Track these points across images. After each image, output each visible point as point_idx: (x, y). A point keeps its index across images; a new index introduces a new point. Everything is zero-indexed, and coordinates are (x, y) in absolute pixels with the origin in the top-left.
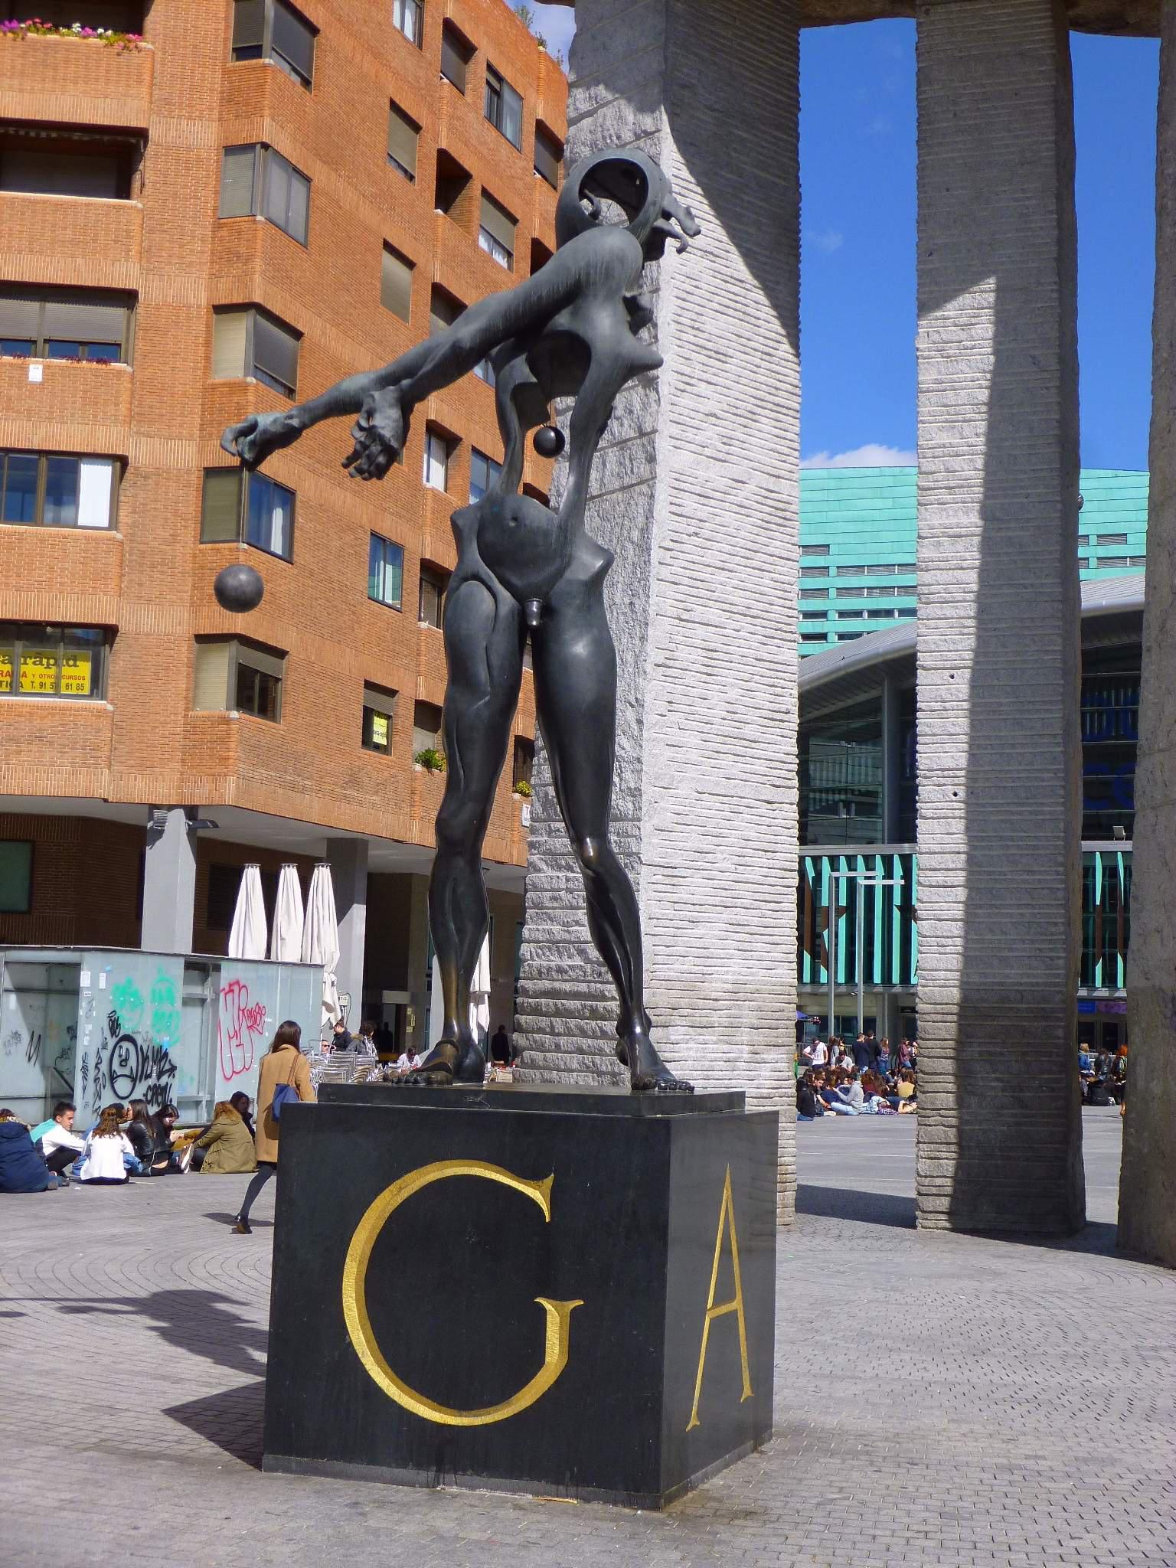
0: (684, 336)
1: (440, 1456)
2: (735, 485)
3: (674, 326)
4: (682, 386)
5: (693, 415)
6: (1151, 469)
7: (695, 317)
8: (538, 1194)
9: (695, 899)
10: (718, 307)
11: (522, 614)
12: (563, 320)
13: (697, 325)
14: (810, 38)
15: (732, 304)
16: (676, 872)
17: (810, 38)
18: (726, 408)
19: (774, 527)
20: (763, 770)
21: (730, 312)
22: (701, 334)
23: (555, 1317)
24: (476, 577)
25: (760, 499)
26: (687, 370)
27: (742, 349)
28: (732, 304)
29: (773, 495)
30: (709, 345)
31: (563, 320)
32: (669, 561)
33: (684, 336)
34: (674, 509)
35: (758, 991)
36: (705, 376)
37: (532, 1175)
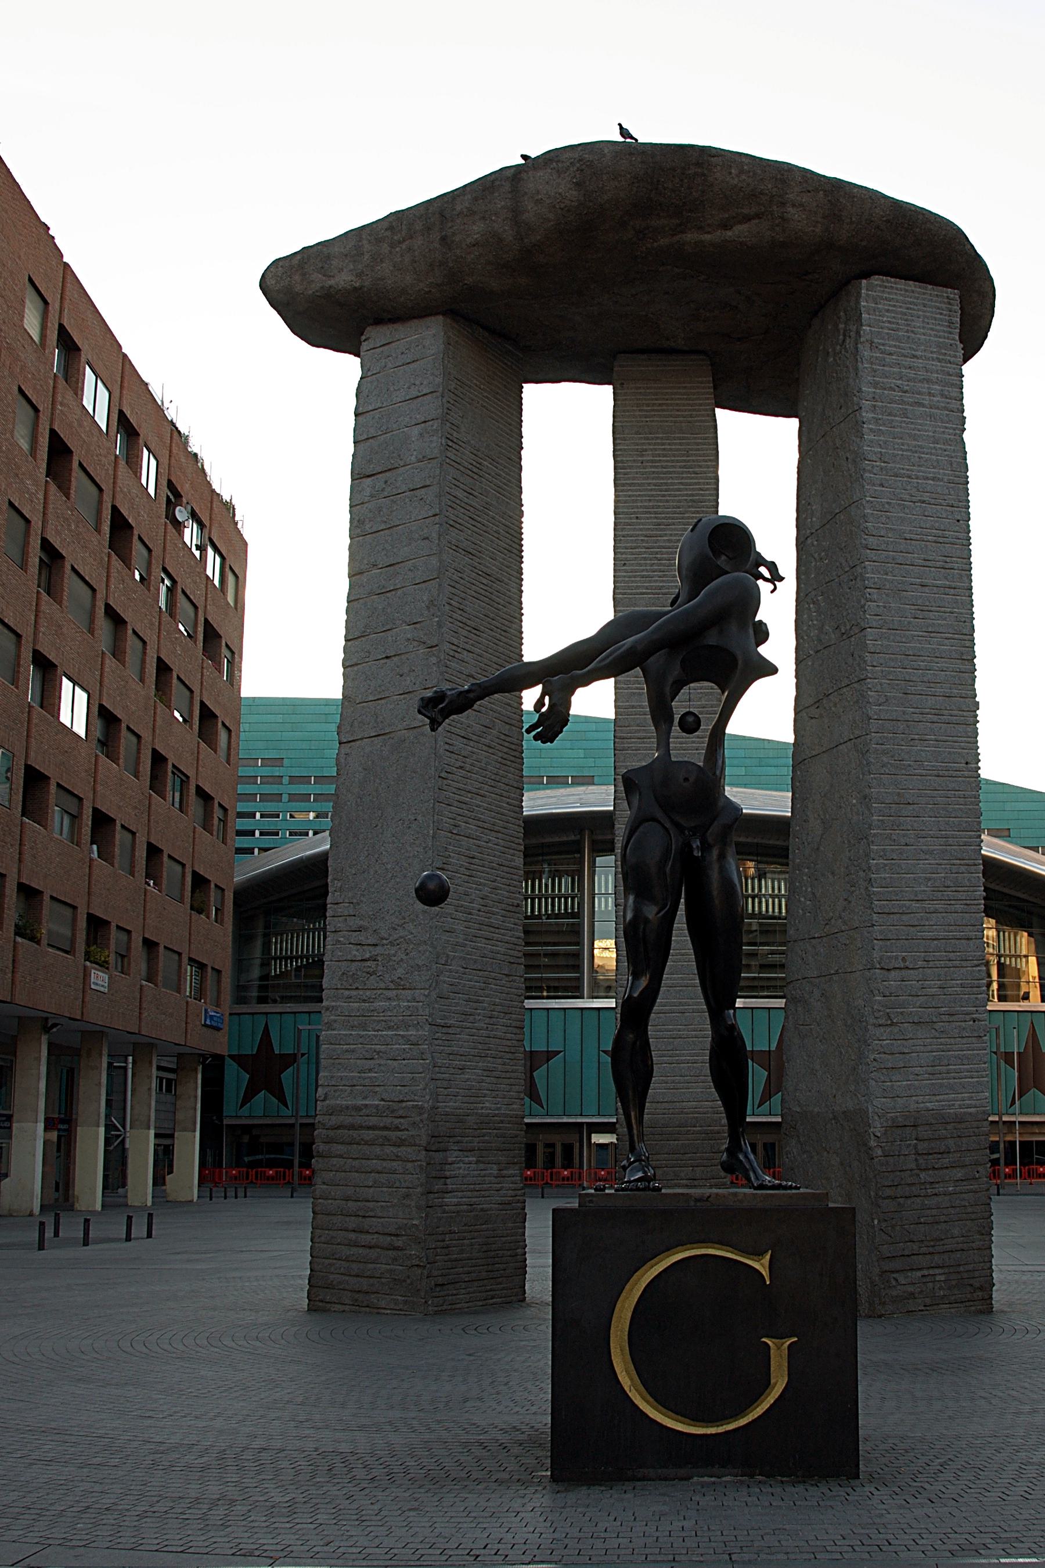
0: (455, 615)
1: (683, 1458)
2: (485, 729)
3: (447, 607)
4: (452, 653)
5: (459, 675)
6: (724, 733)
7: (460, 601)
8: (761, 1265)
9: (462, 1051)
10: (475, 594)
11: (687, 847)
12: (712, 638)
13: (462, 607)
14: (533, 394)
15: (483, 592)
16: (450, 1031)
17: (533, 394)
18: (480, 671)
19: (509, 763)
20: (502, 950)
21: (482, 598)
22: (464, 614)
23: (778, 1352)
24: (654, 820)
25: (501, 742)
26: (456, 642)
27: (488, 626)
28: (483, 592)
29: (508, 739)
30: (469, 622)
31: (712, 638)
32: (445, 788)
33: (455, 615)
34: (447, 747)
35: (502, 1122)
36: (468, 647)
37: (758, 1254)
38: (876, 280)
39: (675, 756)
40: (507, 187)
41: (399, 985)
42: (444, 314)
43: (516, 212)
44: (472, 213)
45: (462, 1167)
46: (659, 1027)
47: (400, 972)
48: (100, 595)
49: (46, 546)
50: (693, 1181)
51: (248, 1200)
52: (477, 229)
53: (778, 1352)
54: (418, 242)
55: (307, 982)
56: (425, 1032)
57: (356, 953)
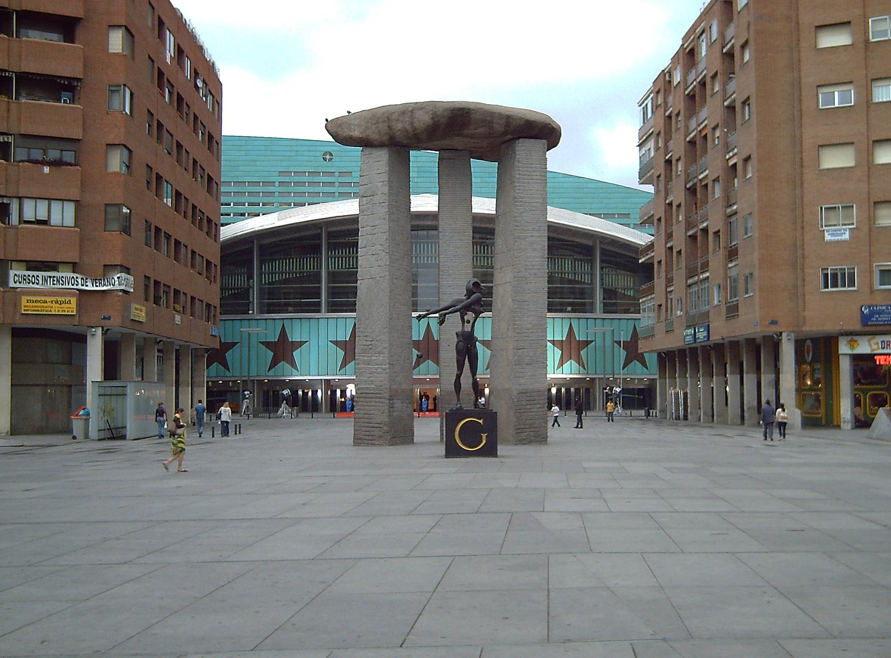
8: (481, 421)
23: (484, 436)
38: (521, 140)
39: (466, 330)
40: (409, 114)
41: (379, 353)
42: (387, 146)
43: (412, 124)
44: (398, 120)
45: (398, 404)
46: (463, 380)
47: (380, 349)
48: (155, 117)
49: (159, 122)
50: (468, 406)
51: (298, 419)
52: (399, 126)
53: (484, 436)
54: (380, 125)
55: (535, 436)
56: (387, 366)
57: (365, 343)
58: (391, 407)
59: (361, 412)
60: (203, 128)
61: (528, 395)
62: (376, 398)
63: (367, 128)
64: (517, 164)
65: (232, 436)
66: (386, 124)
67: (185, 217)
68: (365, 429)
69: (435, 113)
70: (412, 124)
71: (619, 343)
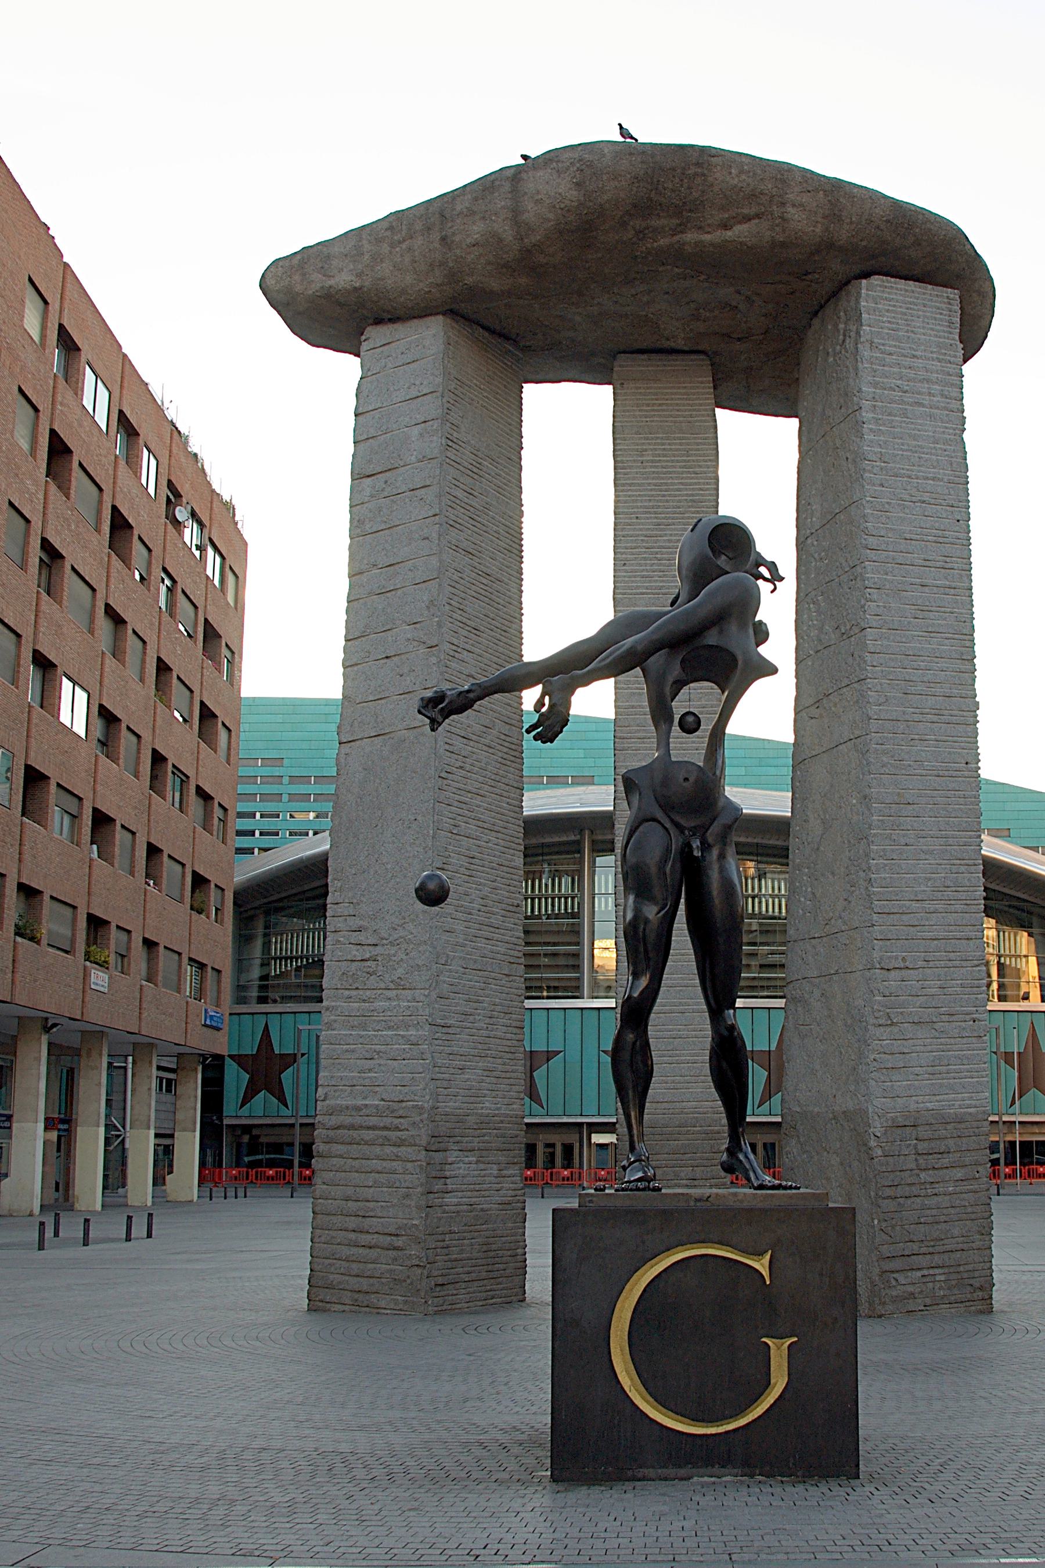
8: (761, 1265)
38: (876, 280)
40: (507, 187)
41: (399, 985)
43: (516, 212)
45: (462, 1167)
46: (659, 1026)
48: (101, 595)
49: (46, 545)
50: (692, 1178)
52: (477, 229)
53: (779, 1351)
54: (419, 242)
55: (307, 981)
56: (425, 1031)
57: (356, 953)
58: (437, 1177)
59: (337, 1191)
60: (229, 654)
61: (923, 1132)
62: (387, 1142)
63: (377, 258)
64: (865, 352)
65: (139, 1246)
66: (436, 236)
67: (181, 810)
68: (346, 1251)
69: (591, 165)
70: (516, 212)
71: (1008, 1057)
